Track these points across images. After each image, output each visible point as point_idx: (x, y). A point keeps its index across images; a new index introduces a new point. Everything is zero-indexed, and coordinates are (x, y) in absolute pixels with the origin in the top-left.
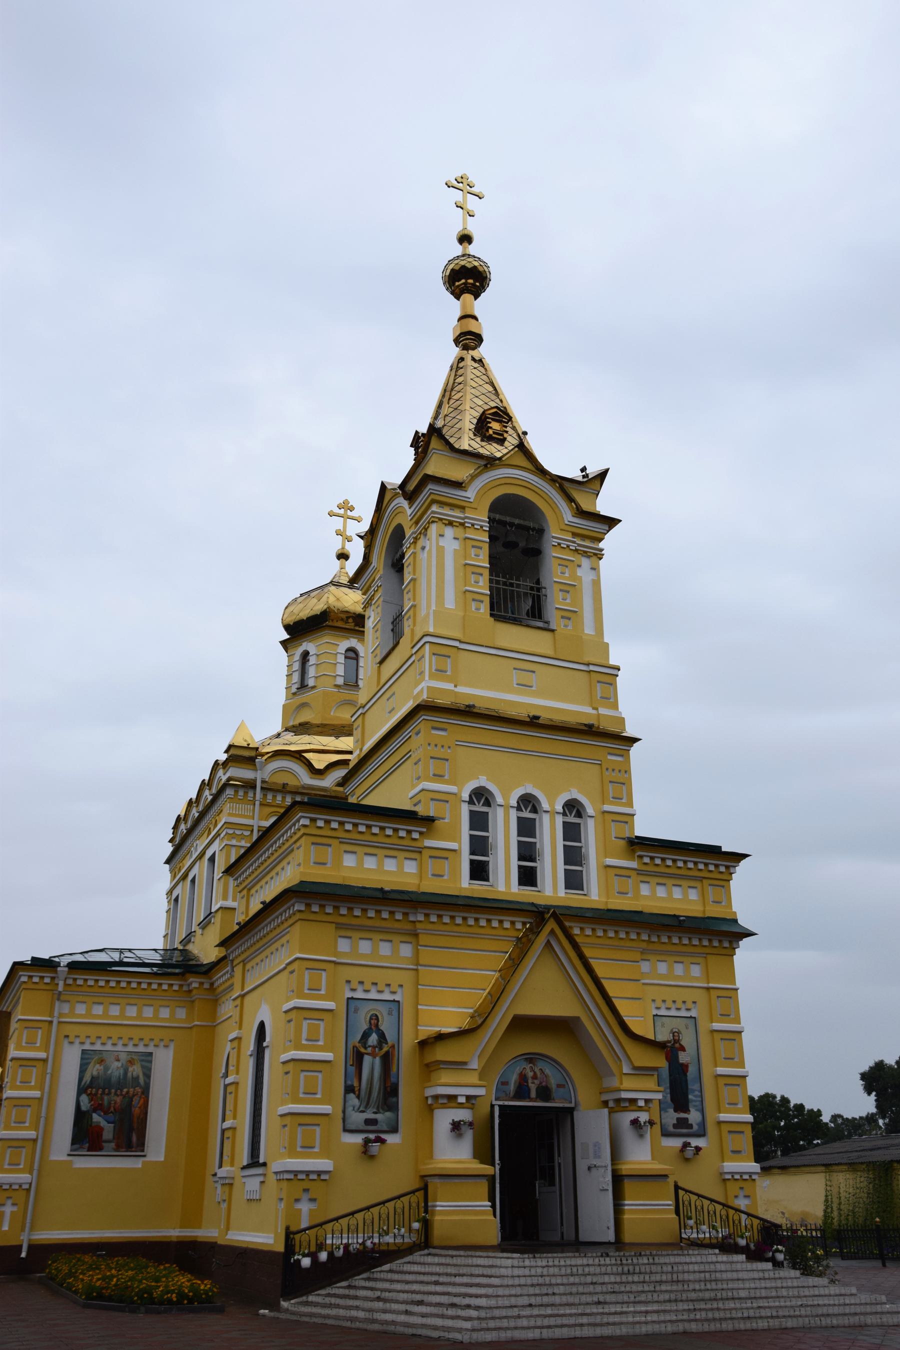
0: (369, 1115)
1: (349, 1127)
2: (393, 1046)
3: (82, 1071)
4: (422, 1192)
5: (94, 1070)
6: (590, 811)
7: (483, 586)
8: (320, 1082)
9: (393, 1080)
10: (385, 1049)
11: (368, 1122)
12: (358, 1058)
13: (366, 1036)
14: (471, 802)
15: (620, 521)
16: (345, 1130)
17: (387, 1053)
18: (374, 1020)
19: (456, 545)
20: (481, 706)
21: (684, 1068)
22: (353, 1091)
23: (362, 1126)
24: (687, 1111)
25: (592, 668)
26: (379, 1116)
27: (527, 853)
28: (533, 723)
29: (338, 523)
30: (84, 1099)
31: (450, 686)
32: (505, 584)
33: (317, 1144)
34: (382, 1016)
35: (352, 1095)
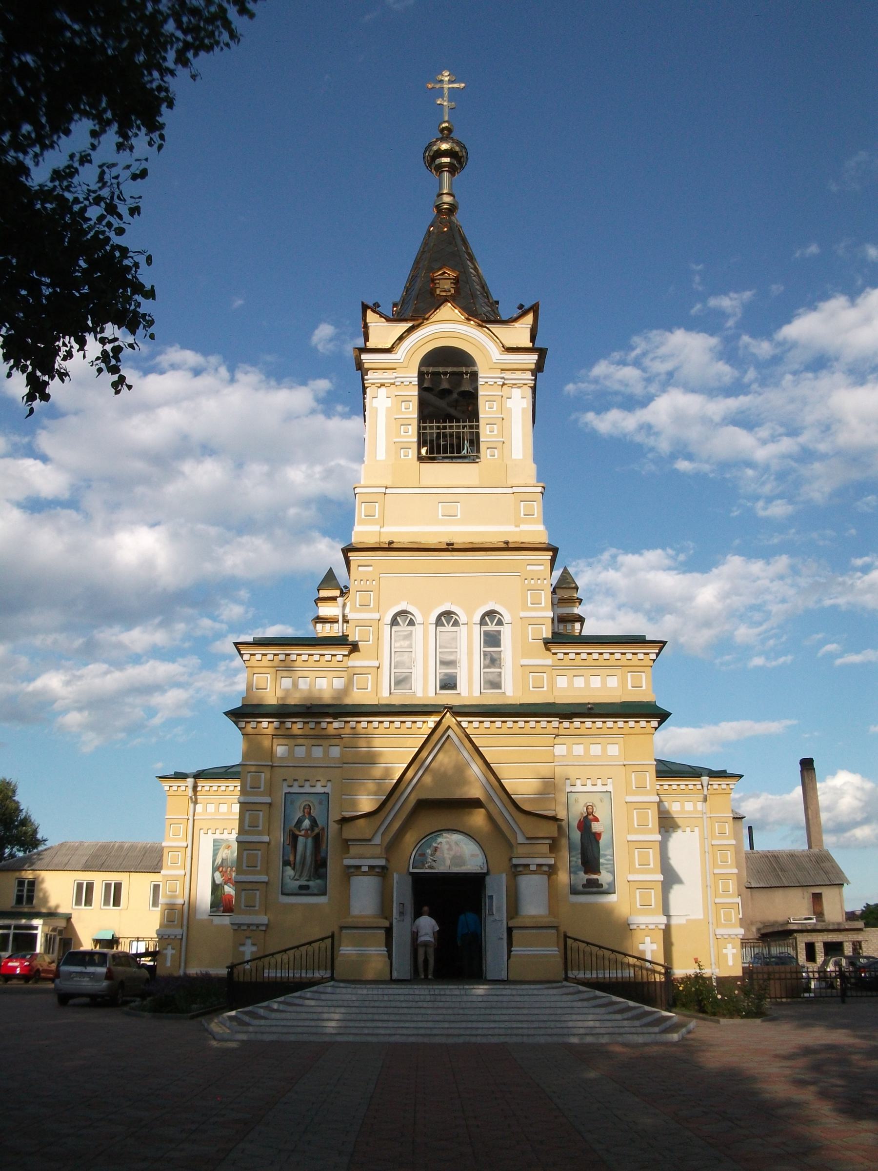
0: (304, 883)
1: (286, 891)
2: (323, 829)
3: (215, 855)
4: (330, 940)
6: (507, 617)
7: (411, 434)
8: (259, 858)
9: (323, 854)
10: (317, 831)
11: (301, 887)
13: (300, 822)
14: (483, 622)
15: (226, 713)
16: (283, 894)
17: (318, 834)
19: (389, 403)
20: (458, 541)
21: (597, 836)
22: (289, 864)
23: (297, 891)
24: (598, 872)
25: (515, 489)
26: (311, 883)
28: (450, 548)
30: (218, 875)
31: (376, 528)
32: (438, 428)
33: (257, 905)
34: (314, 805)
35: (289, 868)
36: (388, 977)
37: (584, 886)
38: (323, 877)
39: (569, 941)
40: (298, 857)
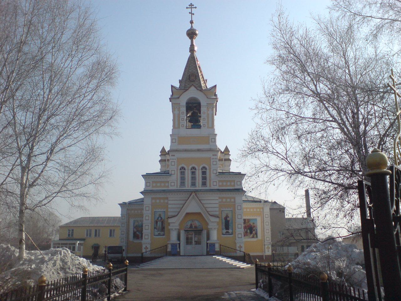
0: (159, 233)
3: (134, 224)
5: (136, 224)
11: (159, 234)
12: (157, 222)
13: (158, 218)
15: (163, 147)
16: (154, 235)
18: (160, 215)
21: (228, 221)
24: (228, 229)
27: (193, 178)
29: (189, 10)
38: (164, 231)
40: (158, 226)
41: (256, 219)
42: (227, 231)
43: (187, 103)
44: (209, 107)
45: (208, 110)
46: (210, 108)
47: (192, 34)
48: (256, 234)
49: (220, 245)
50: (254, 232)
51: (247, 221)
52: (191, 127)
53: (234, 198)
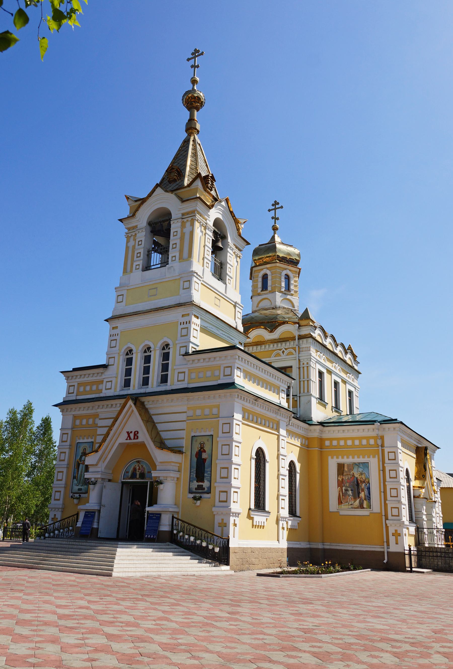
0: (80, 487)
22: (75, 478)
24: (203, 481)
26: (82, 487)
36: (115, 536)
37: (196, 489)
39: (175, 520)
41: (366, 465)
42: (201, 484)
43: (150, 224)
44: (185, 220)
45: (183, 226)
46: (187, 221)
47: (192, 102)
48: (368, 498)
49: (173, 517)
50: (362, 495)
51: (346, 469)
52: (159, 266)
53: (218, 407)
